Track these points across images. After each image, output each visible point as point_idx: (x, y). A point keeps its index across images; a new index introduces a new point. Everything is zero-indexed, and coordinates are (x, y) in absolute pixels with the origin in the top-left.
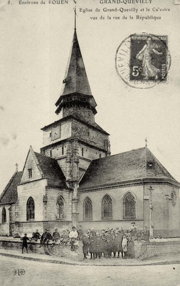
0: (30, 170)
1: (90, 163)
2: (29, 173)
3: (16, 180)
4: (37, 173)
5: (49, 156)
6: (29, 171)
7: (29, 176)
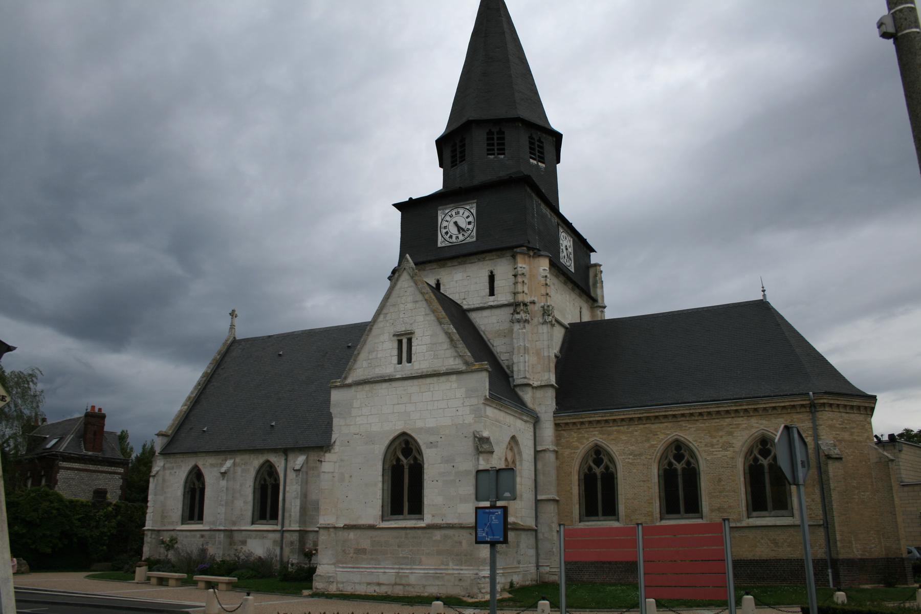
1: (559, 334)
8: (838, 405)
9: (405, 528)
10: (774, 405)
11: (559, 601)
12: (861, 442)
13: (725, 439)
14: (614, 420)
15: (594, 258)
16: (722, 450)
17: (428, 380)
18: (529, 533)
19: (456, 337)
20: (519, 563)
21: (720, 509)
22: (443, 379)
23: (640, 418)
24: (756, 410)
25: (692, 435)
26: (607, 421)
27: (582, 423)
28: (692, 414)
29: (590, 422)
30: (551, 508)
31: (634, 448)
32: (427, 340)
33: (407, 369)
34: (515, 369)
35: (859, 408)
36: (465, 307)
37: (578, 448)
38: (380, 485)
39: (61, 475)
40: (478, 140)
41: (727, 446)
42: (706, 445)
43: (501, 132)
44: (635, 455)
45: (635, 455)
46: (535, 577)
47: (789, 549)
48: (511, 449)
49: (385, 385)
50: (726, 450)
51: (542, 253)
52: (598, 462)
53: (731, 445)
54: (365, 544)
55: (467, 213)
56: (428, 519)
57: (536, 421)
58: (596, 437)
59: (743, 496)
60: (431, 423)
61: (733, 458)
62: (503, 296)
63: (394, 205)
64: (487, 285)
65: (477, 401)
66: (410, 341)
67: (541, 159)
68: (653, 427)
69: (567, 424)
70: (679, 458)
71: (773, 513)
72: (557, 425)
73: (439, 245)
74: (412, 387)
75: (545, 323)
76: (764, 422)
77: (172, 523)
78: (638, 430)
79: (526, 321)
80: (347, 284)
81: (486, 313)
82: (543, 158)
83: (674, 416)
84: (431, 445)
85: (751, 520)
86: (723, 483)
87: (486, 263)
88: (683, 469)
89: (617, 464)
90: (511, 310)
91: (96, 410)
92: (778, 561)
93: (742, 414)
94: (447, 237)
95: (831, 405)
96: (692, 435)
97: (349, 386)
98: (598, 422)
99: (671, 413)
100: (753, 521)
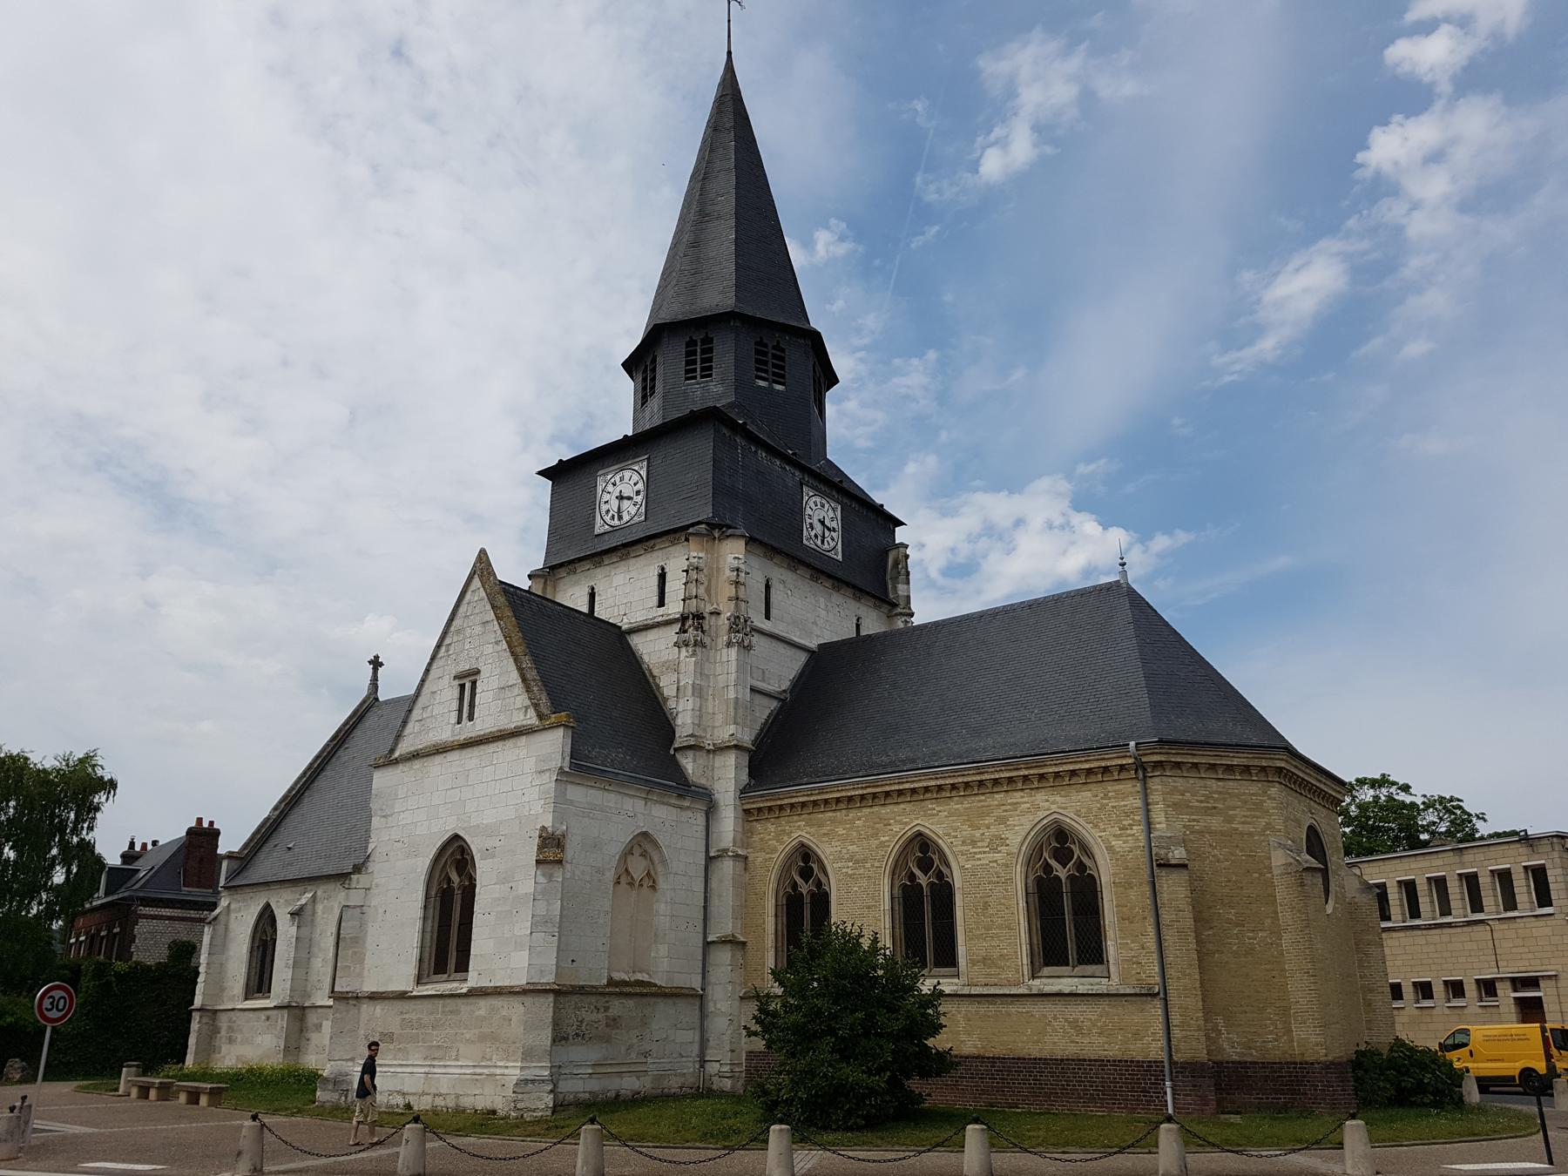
0: (468, 681)
1: (803, 658)
2: (461, 699)
3: (369, 734)
4: (504, 695)
5: (585, 609)
6: (462, 687)
7: (460, 711)
8: (1195, 766)
9: (441, 996)
10: (1071, 767)
11: (389, 1155)
12: (1250, 834)
13: (993, 830)
14: (826, 801)
15: (901, 535)
16: (988, 848)
17: (491, 748)
18: (681, 1003)
19: (532, 674)
20: (646, 1054)
21: (985, 960)
22: (510, 743)
23: (863, 797)
24: (1042, 777)
25: (942, 822)
26: (815, 803)
27: (781, 808)
28: (940, 788)
29: (792, 806)
30: (723, 958)
32: (495, 683)
33: (470, 730)
34: (679, 721)
35: (1246, 769)
36: (624, 627)
37: (774, 850)
38: (418, 925)
39: (142, 928)
40: (670, 362)
41: (997, 842)
43: (708, 340)
45: (857, 862)
46: (691, 1080)
47: (1102, 1040)
48: (644, 854)
49: (438, 759)
50: (995, 850)
51: (738, 532)
52: (1063, 856)
53: (1003, 841)
54: (394, 1025)
55: (636, 477)
56: (474, 979)
57: (711, 809)
58: (800, 830)
59: (1024, 937)
60: (489, 818)
61: (1007, 866)
62: (674, 608)
63: (539, 473)
64: (655, 589)
65: (549, 780)
66: (474, 683)
68: (884, 810)
69: (760, 810)
70: (1063, 856)
71: (1079, 969)
73: (597, 531)
74: (472, 757)
75: (729, 644)
76: (1058, 798)
77: (232, 998)
78: (860, 818)
79: (703, 646)
80: (1107, 574)
81: (652, 635)
82: (783, 376)
83: (914, 791)
84: (488, 853)
85: (1037, 982)
87: (655, 554)
88: (1071, 878)
89: (1096, 851)
90: (677, 627)
91: (205, 825)
92: (1081, 1061)
93: (1020, 785)
94: (607, 518)
95: (1178, 765)
96: (942, 822)
97: (396, 762)
98: (804, 804)
99: (907, 786)
100: (1037, 985)
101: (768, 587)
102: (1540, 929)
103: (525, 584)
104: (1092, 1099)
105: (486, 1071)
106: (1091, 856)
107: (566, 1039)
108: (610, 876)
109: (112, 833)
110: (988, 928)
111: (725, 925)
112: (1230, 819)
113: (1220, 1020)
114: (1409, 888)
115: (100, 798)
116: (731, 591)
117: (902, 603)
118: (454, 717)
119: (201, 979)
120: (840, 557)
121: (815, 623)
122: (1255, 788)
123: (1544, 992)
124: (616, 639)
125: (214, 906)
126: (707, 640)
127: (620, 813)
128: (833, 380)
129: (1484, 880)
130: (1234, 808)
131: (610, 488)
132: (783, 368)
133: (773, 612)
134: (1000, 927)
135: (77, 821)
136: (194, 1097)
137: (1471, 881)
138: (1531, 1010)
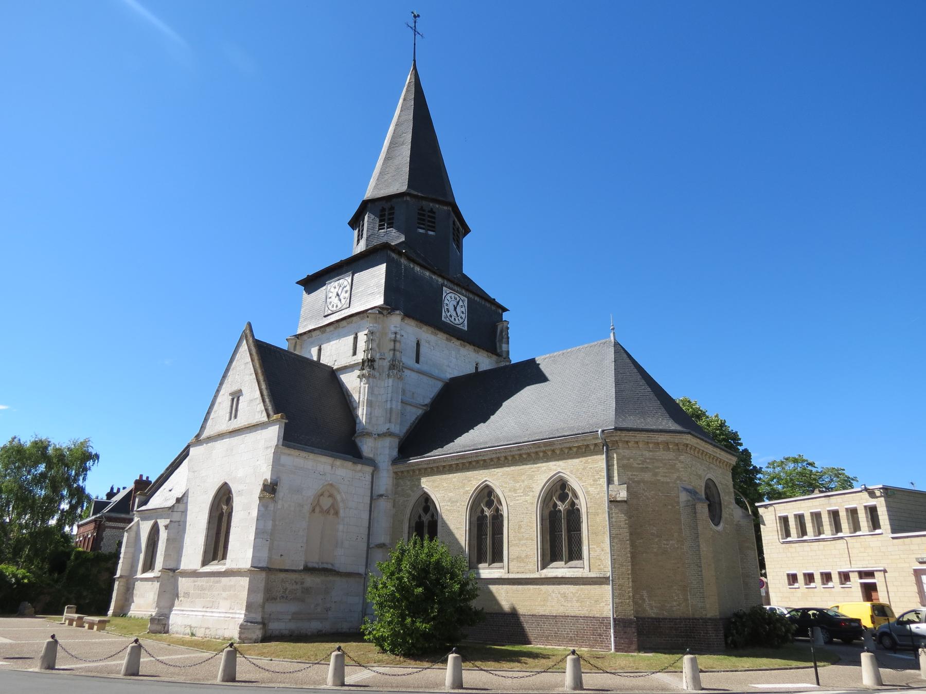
2: (232, 406)
6: (233, 399)
7: (231, 413)
12: (668, 483)
15: (505, 316)
31: (451, 494)
42: (510, 491)
44: (453, 502)
45: (453, 502)
47: (578, 604)
50: (526, 495)
52: (563, 498)
53: (530, 488)
67: (433, 228)
70: (563, 498)
72: (396, 473)
79: (374, 377)
84: (240, 493)
86: (523, 530)
91: (144, 478)
100: (549, 572)
101: (418, 344)
102: (874, 542)
103: (284, 346)
104: (571, 640)
105: (231, 615)
106: (576, 496)
107: (275, 599)
108: (307, 508)
109: (96, 485)
110: (520, 540)
111: (382, 537)
112: (656, 474)
113: (645, 594)
114: (800, 518)
115: (89, 464)
116: (391, 345)
117: (504, 355)
118: (228, 418)
119: (121, 561)
120: (466, 328)
121: (449, 366)
122: (671, 455)
123: (878, 580)
124: (332, 375)
125: (131, 520)
126: (377, 374)
127: (319, 469)
128: (467, 230)
129: (843, 515)
130: (659, 468)
131: (332, 289)
132: (434, 223)
133: (421, 359)
134: (527, 539)
135: (77, 475)
136: (91, 628)
137: (835, 515)
138: (869, 591)
